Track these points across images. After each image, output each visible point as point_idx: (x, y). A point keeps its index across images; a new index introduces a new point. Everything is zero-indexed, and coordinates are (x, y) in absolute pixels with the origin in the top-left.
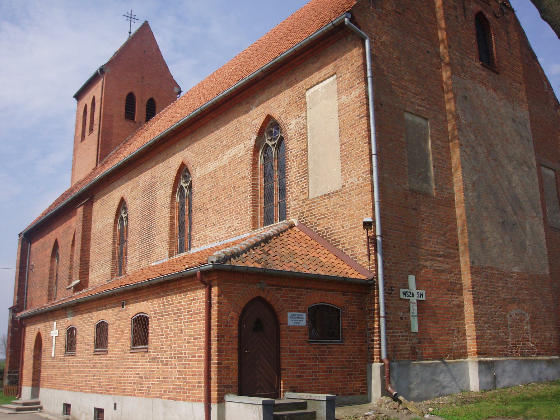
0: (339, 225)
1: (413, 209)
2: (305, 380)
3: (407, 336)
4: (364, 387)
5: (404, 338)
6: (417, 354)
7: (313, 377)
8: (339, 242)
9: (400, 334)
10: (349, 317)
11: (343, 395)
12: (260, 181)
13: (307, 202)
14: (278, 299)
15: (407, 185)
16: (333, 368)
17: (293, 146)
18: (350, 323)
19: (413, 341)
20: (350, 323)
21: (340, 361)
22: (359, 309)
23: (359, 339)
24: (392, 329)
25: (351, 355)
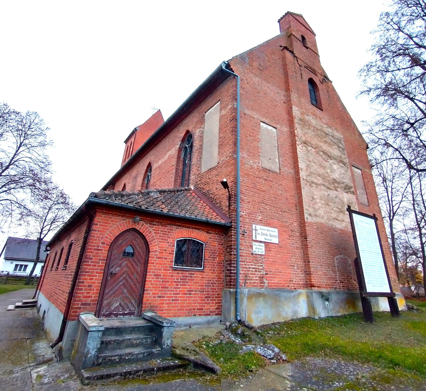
0: (214, 188)
1: (264, 179)
2: (165, 300)
3: (256, 269)
4: (220, 309)
5: (254, 270)
6: (265, 283)
7: (174, 298)
8: (213, 198)
9: (250, 266)
10: (211, 250)
11: (200, 315)
12: (181, 167)
13: (199, 176)
14: (151, 232)
15: (260, 164)
16: (193, 291)
17: (196, 144)
18: (211, 255)
19: (262, 273)
20: (211, 255)
21: (199, 286)
22: (219, 244)
23: (218, 268)
24: (244, 262)
25: (210, 281)
